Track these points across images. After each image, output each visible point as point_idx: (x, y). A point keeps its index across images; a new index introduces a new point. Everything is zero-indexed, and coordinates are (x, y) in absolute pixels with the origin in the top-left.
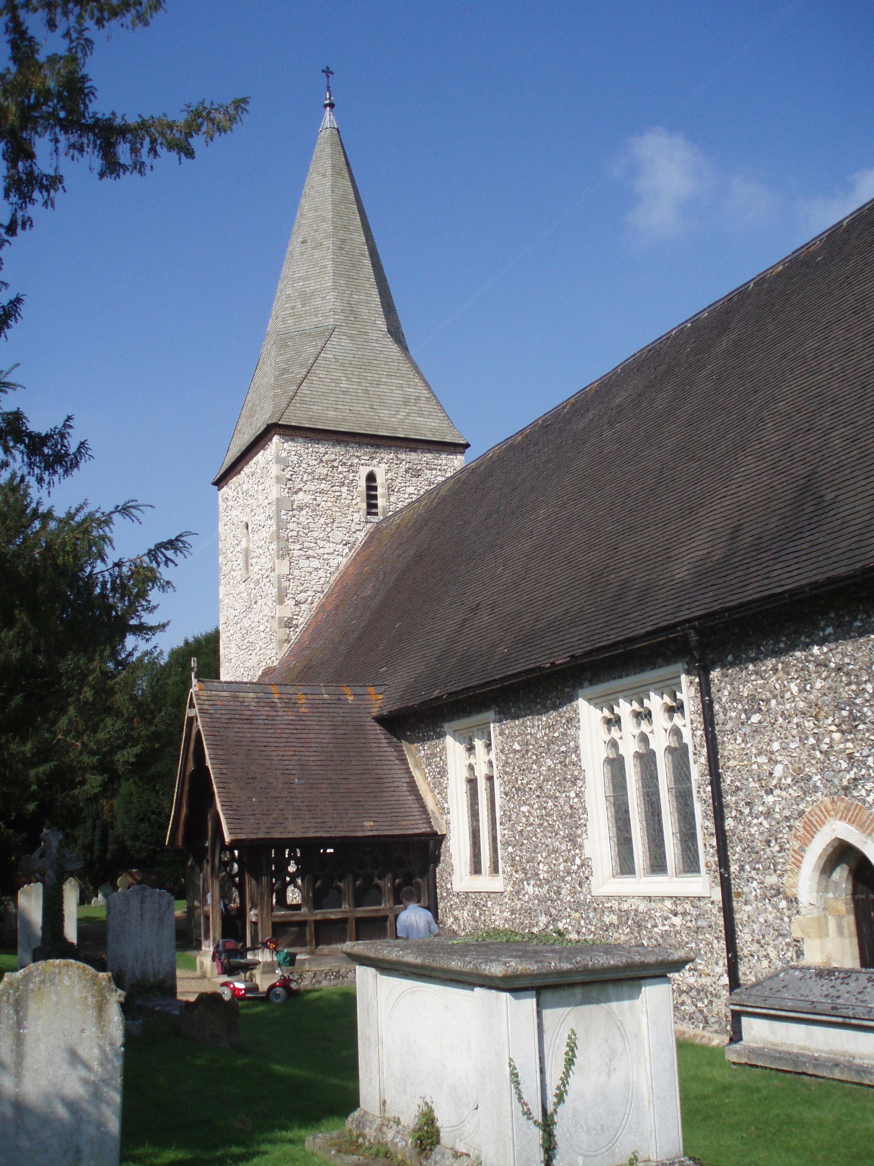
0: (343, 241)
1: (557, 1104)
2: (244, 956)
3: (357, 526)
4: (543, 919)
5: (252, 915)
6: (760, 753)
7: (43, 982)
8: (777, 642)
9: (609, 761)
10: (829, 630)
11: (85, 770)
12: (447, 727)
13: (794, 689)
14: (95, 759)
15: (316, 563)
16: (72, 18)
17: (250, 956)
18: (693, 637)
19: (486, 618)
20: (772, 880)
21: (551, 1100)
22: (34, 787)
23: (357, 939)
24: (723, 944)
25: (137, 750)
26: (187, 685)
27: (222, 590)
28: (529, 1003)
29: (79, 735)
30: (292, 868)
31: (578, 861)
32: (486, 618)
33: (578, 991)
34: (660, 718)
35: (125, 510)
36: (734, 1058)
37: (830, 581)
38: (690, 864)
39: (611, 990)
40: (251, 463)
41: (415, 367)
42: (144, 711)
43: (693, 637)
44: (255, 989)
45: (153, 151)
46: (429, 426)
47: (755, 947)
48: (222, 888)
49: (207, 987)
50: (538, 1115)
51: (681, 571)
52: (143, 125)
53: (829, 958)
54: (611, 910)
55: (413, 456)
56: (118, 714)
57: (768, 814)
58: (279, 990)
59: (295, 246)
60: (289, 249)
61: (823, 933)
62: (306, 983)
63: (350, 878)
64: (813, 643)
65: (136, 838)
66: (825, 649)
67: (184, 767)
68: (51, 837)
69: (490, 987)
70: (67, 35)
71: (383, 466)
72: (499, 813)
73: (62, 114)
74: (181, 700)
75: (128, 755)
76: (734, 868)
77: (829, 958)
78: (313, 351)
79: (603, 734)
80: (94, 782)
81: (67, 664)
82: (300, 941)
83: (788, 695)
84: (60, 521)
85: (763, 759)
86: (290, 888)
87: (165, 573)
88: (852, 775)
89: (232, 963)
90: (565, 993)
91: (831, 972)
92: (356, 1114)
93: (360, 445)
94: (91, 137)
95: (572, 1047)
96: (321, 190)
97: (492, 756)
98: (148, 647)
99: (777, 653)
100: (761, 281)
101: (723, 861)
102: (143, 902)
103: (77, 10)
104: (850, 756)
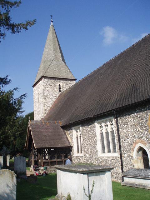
0: (54, 45)
1: (91, 193)
2: (38, 168)
3: (57, 94)
4: (90, 161)
5: (40, 161)
6: (126, 132)
7: (2, 173)
8: (129, 113)
9: (101, 133)
10: (138, 111)
11: (11, 136)
12: (73, 128)
13: (132, 120)
14: (12, 134)
15: (50, 100)
16: (6, 6)
17: (39, 168)
18: (115, 112)
19: (79, 110)
20: (129, 154)
21: (90, 192)
22: (2, 139)
23: (58, 165)
24: (120, 165)
25: (20, 132)
26: (28, 121)
27: (34, 105)
28: (86, 176)
29: (9, 130)
30: (46, 153)
31: (96, 151)
32: (79, 110)
33: (95, 173)
34: (109, 126)
35: (16, 89)
36: (122, 184)
37: (138, 102)
38: (115, 151)
39: (100, 173)
40: (39, 83)
41: (67, 66)
42: (21, 126)
43: (115, 112)
44: (40, 173)
45: (21, 29)
46: (70, 76)
47: (126, 165)
48: (34, 156)
49: (32, 173)
50: (88, 195)
51: (112, 101)
52: (19, 25)
53: (139, 167)
54: (101, 159)
55: (67, 81)
56: (16, 126)
57: (128, 142)
58: (44, 174)
59: (46, 46)
60: (45, 46)
61: (138, 163)
62: (49, 172)
63: (57, 154)
64: (135, 113)
65: (20, 148)
66: (137, 114)
67: (27, 135)
68: (5, 148)
69: (80, 173)
70: (5, 9)
71: (62, 83)
72: (82, 143)
73: (5, 23)
74: (27, 124)
75: (18, 133)
76: (122, 152)
77: (139, 167)
78: (50, 64)
79: (99, 129)
80: (12, 138)
81: (7, 118)
82: (48, 165)
83: (131, 122)
84: (6, 93)
85: (127, 133)
86: (46, 156)
87: (23, 100)
88: (142, 135)
89: (36, 169)
90: (92, 174)
91: (139, 169)
92: (57, 195)
93: (58, 80)
94: (10, 27)
95: (94, 183)
96: (51, 36)
97: (81, 133)
98: (21, 115)
99: (129, 115)
100: (126, 51)
101: (120, 151)
102: (21, 159)
103: (7, 5)
104: (142, 132)
